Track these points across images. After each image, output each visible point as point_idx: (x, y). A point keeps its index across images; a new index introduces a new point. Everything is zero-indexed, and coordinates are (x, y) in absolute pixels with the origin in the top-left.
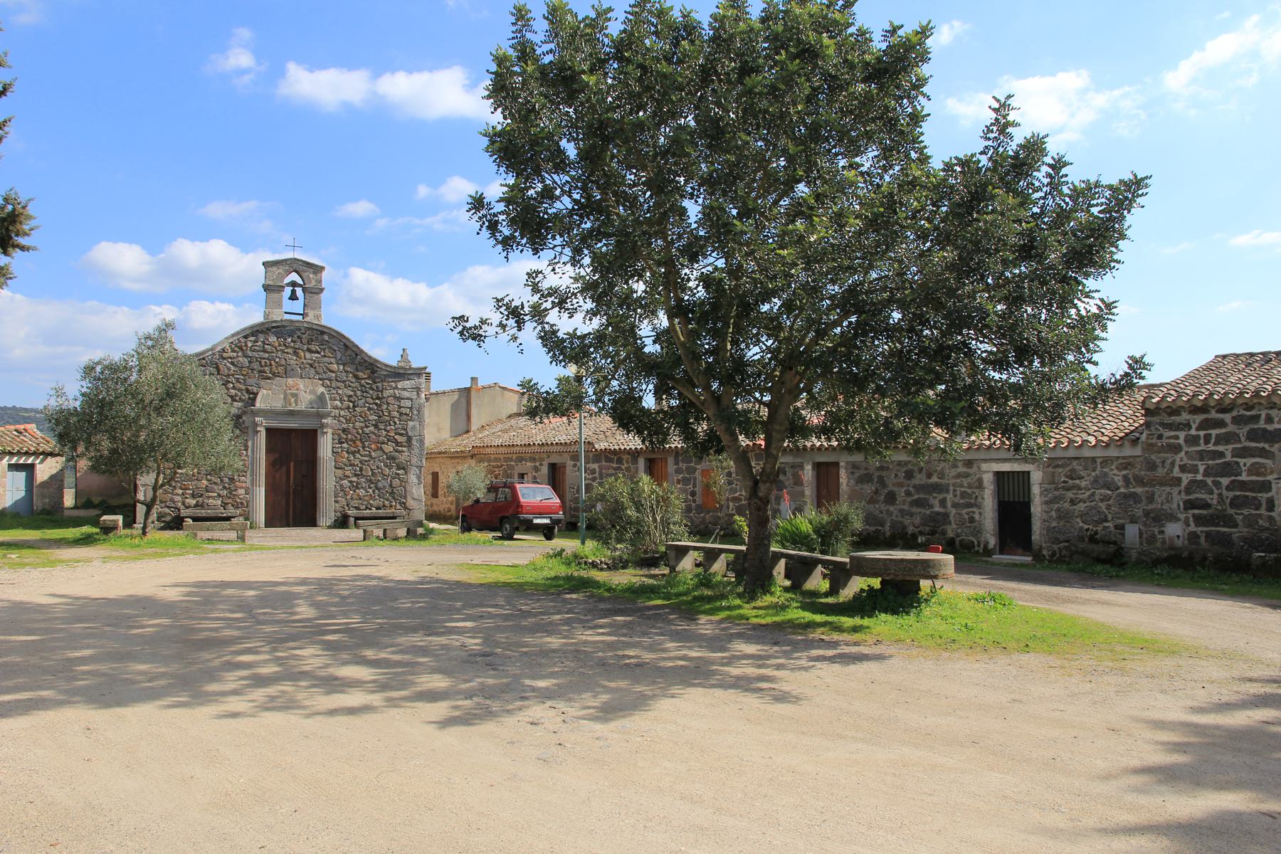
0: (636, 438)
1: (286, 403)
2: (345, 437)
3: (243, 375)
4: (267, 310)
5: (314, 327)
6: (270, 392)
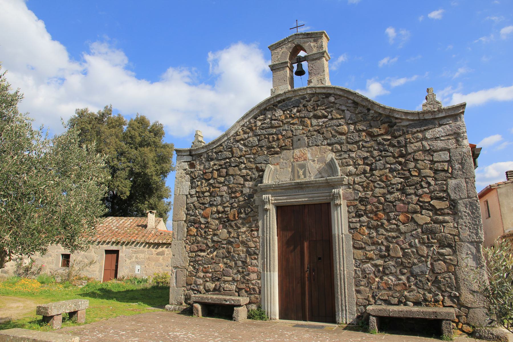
1: (294, 176)
2: (363, 208)
3: (254, 154)
5: (318, 91)
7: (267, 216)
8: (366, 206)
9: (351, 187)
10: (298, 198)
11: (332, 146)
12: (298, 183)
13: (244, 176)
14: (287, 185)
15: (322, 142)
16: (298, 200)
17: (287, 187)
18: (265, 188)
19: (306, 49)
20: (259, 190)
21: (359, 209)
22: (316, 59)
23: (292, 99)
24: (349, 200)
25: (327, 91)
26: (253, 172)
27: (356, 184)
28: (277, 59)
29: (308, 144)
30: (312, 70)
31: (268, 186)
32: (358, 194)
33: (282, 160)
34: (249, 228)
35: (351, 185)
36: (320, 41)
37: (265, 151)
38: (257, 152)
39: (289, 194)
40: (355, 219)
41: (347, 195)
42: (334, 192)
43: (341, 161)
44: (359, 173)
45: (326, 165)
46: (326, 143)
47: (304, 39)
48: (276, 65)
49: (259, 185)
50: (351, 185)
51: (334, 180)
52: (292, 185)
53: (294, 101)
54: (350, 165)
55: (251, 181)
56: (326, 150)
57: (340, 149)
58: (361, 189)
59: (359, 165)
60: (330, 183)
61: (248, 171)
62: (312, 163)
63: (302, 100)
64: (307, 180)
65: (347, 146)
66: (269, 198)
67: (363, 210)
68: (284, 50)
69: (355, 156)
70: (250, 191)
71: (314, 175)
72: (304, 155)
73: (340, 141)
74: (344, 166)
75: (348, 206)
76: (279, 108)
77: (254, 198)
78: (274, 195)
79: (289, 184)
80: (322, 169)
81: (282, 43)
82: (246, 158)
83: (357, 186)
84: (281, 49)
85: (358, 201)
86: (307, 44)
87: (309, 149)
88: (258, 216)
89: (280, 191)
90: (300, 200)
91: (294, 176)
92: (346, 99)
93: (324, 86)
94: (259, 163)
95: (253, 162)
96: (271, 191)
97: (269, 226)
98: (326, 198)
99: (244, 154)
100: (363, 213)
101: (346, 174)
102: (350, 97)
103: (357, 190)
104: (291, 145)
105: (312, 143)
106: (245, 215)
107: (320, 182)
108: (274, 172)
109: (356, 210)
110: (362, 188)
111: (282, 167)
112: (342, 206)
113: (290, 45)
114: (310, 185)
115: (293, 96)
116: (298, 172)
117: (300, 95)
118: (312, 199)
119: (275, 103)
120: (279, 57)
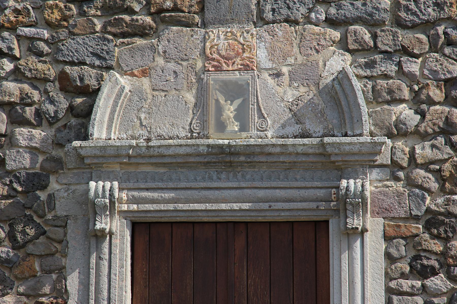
0: (420, 181)
1: (204, 123)
2: (437, 247)
3: (49, 25)
6: (146, 82)
7: (100, 258)
8: (447, 240)
9: (401, 174)
10: (217, 201)
11: (343, 29)
12: (221, 147)
13: (11, 104)
14: (182, 151)
15: (310, 10)
16: (215, 207)
17: (179, 160)
18: (96, 157)
20: (71, 162)
21: (425, 251)
24: (393, 218)
26: (46, 92)
27: (417, 166)
29: (260, 12)
31: (112, 152)
32: (423, 199)
33: (160, 61)
34: (28, 296)
35: (402, 168)
37: (95, 21)
38: (65, 18)
39: (183, 185)
40: (409, 282)
41: (388, 202)
42: (347, 188)
43: (370, 85)
44: (430, 131)
45: (320, 92)
46: (323, 17)
49: (77, 143)
50: (402, 168)
51: (347, 148)
52: (199, 155)
54: (402, 101)
55: (39, 125)
56: (323, 42)
57: (372, 44)
58: (434, 185)
59: (431, 102)
60: (333, 159)
61: (26, 87)
62: (271, 81)
64: (252, 141)
65: (395, 35)
66: (112, 195)
67: (436, 254)
69: (421, 69)
70: (33, 161)
71: (277, 126)
72: (244, 50)
73: (371, 15)
74: (378, 103)
75: (388, 238)
77: (49, 190)
78: (131, 185)
79: (189, 150)
80: (306, 106)
82: (19, 37)
83: (422, 172)
85: (423, 221)
87: (262, 31)
88: (65, 255)
89: (149, 169)
90: (223, 206)
91: (204, 123)
94: (72, 63)
95: (47, 54)
96: (117, 168)
97: (105, 294)
98: (313, 205)
99: (10, 22)
100: (437, 265)
101: (384, 131)
103: (421, 187)
104: (196, 8)
105: (273, 10)
106: (13, 248)
107: (300, 150)
108: (130, 100)
109: (413, 253)
110: (437, 181)
111: (161, 85)
112: (367, 236)
114: (263, 159)
116: (219, 109)
118: (265, 206)
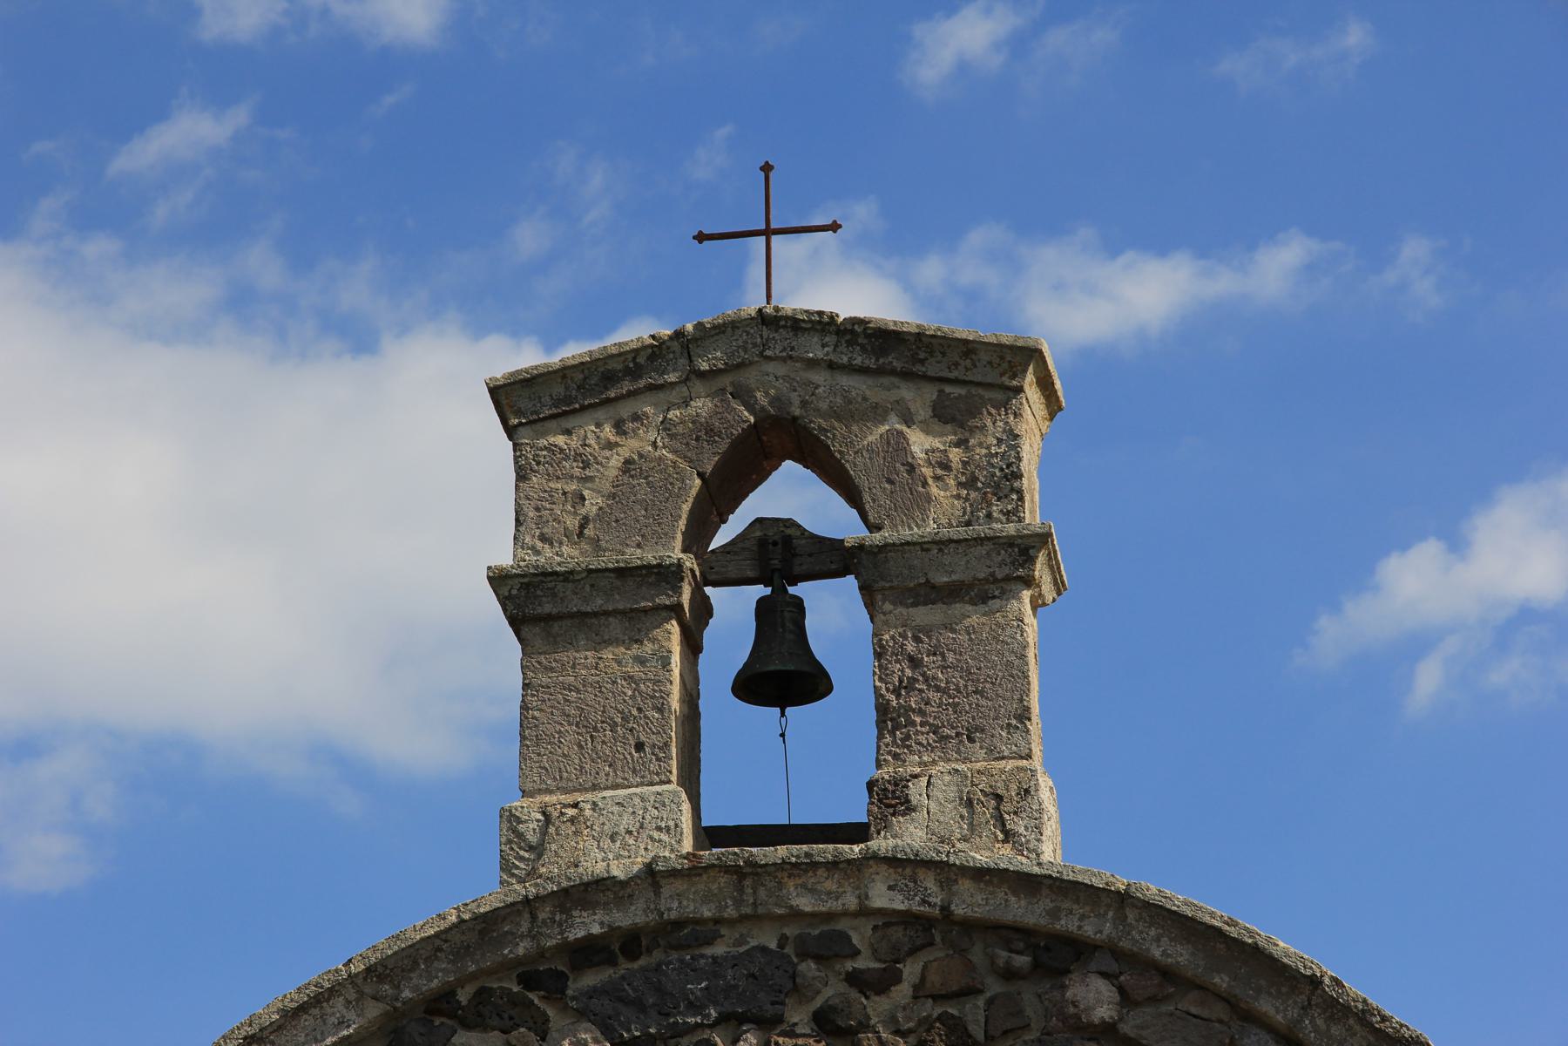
4: (530, 810)
5: (970, 902)
19: (862, 480)
22: (953, 593)
23: (709, 942)
25: (1054, 914)
28: (572, 523)
30: (910, 686)
36: (993, 426)
47: (845, 381)
48: (568, 577)
53: (735, 961)
63: (809, 968)
68: (643, 441)
76: (583, 1014)
81: (634, 372)
84: (619, 427)
86: (876, 434)
92: (1219, 1011)
93: (1024, 863)
102: (1266, 1006)
113: (702, 406)
115: (731, 912)
117: (796, 915)
119: (541, 954)
120: (593, 503)
